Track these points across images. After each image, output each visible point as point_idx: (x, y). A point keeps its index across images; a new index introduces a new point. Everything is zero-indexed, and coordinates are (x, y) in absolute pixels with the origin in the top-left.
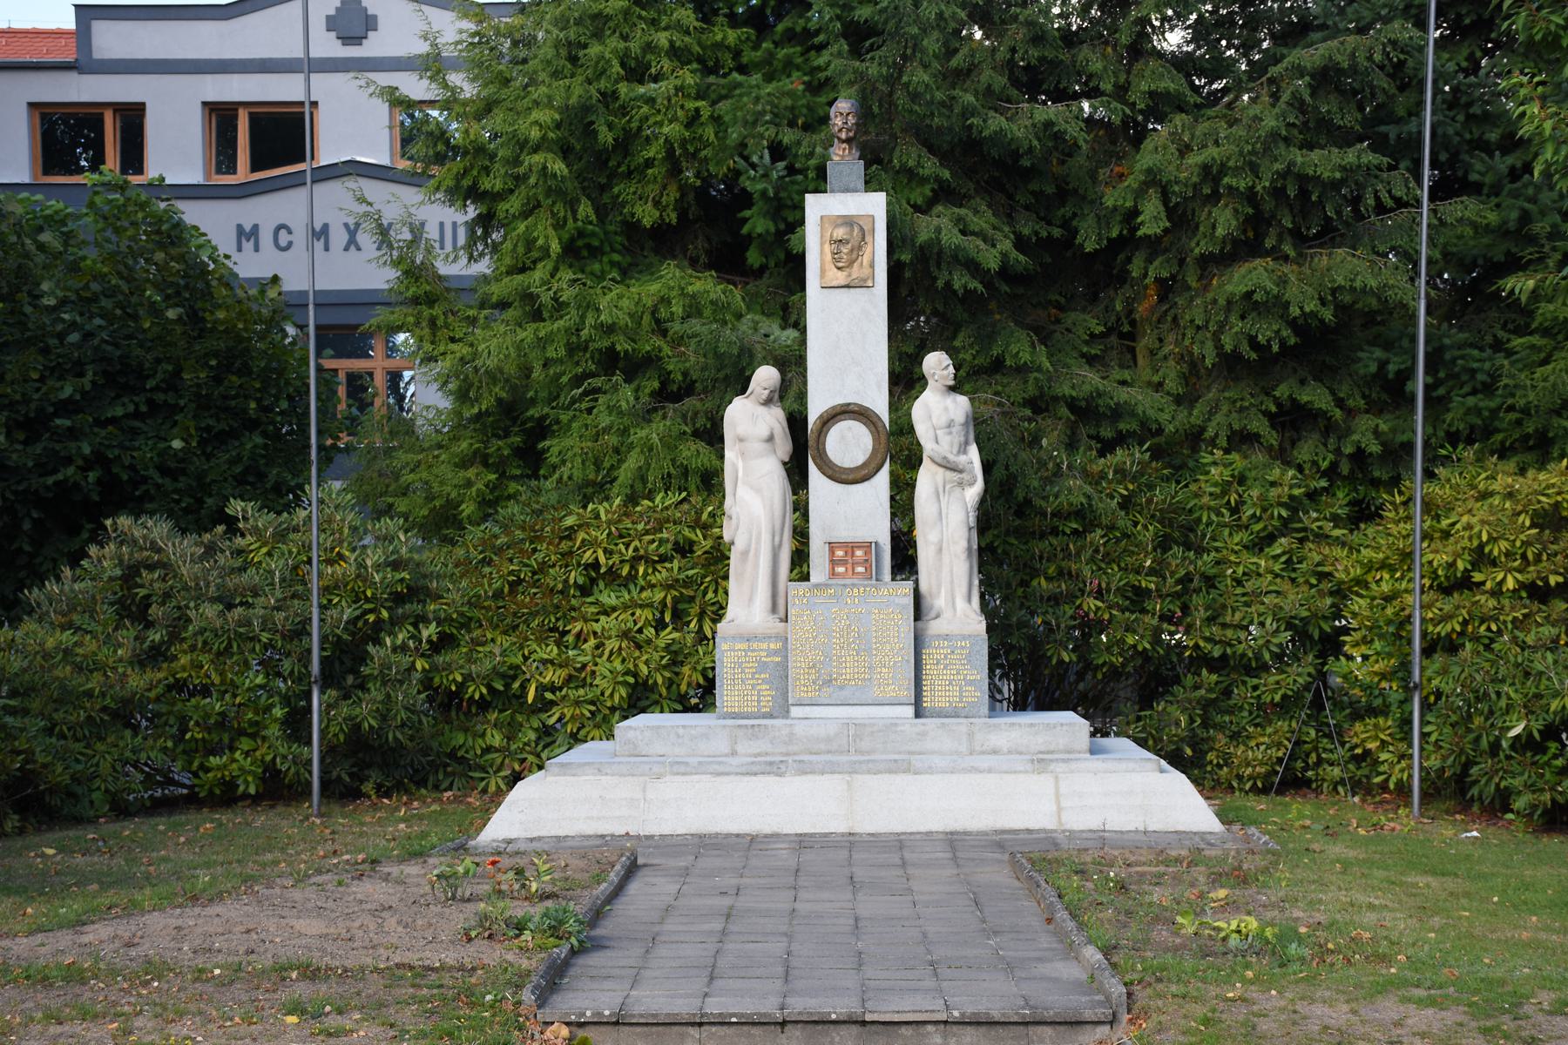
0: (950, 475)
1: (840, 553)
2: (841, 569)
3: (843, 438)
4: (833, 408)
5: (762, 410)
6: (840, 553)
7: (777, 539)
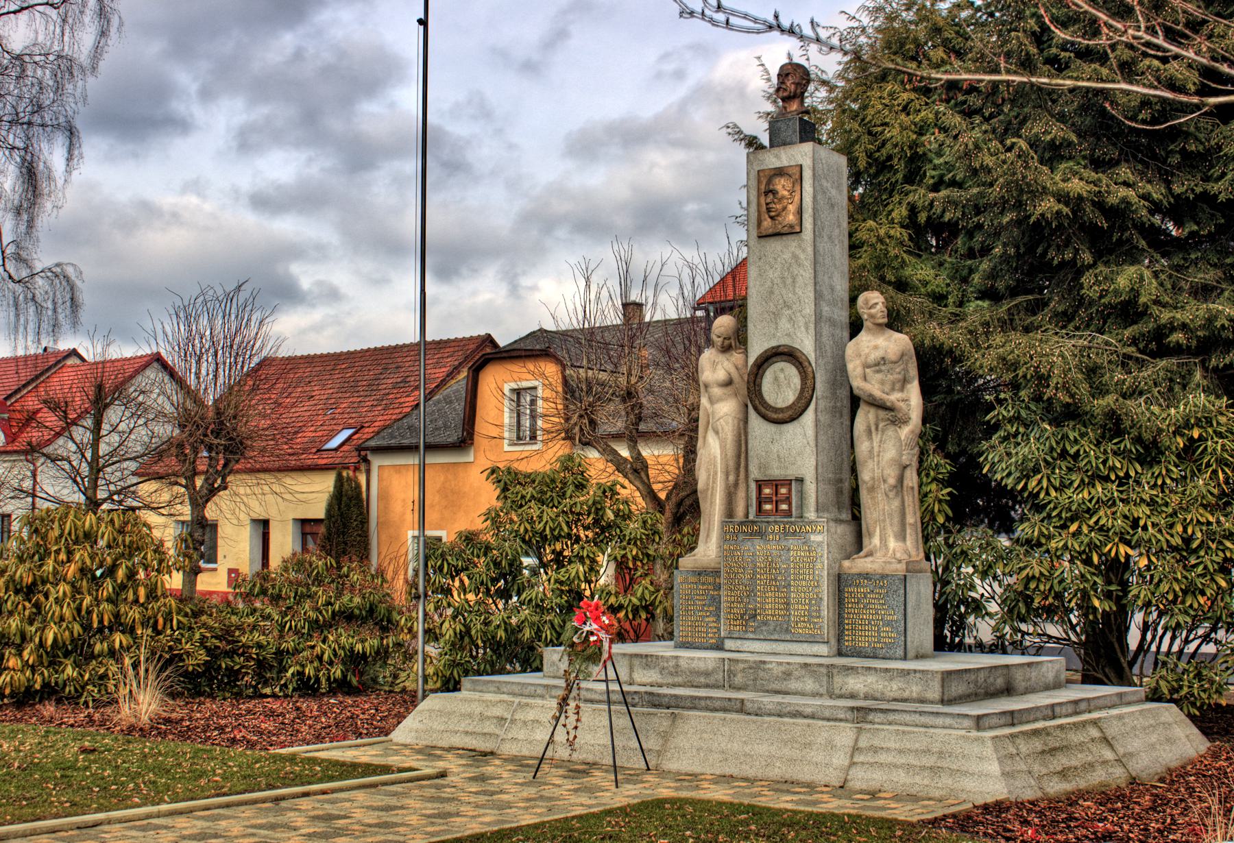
0: (882, 414)
1: (767, 491)
2: (768, 507)
3: (776, 379)
4: (766, 351)
5: (722, 358)
6: (767, 491)
7: (732, 478)
